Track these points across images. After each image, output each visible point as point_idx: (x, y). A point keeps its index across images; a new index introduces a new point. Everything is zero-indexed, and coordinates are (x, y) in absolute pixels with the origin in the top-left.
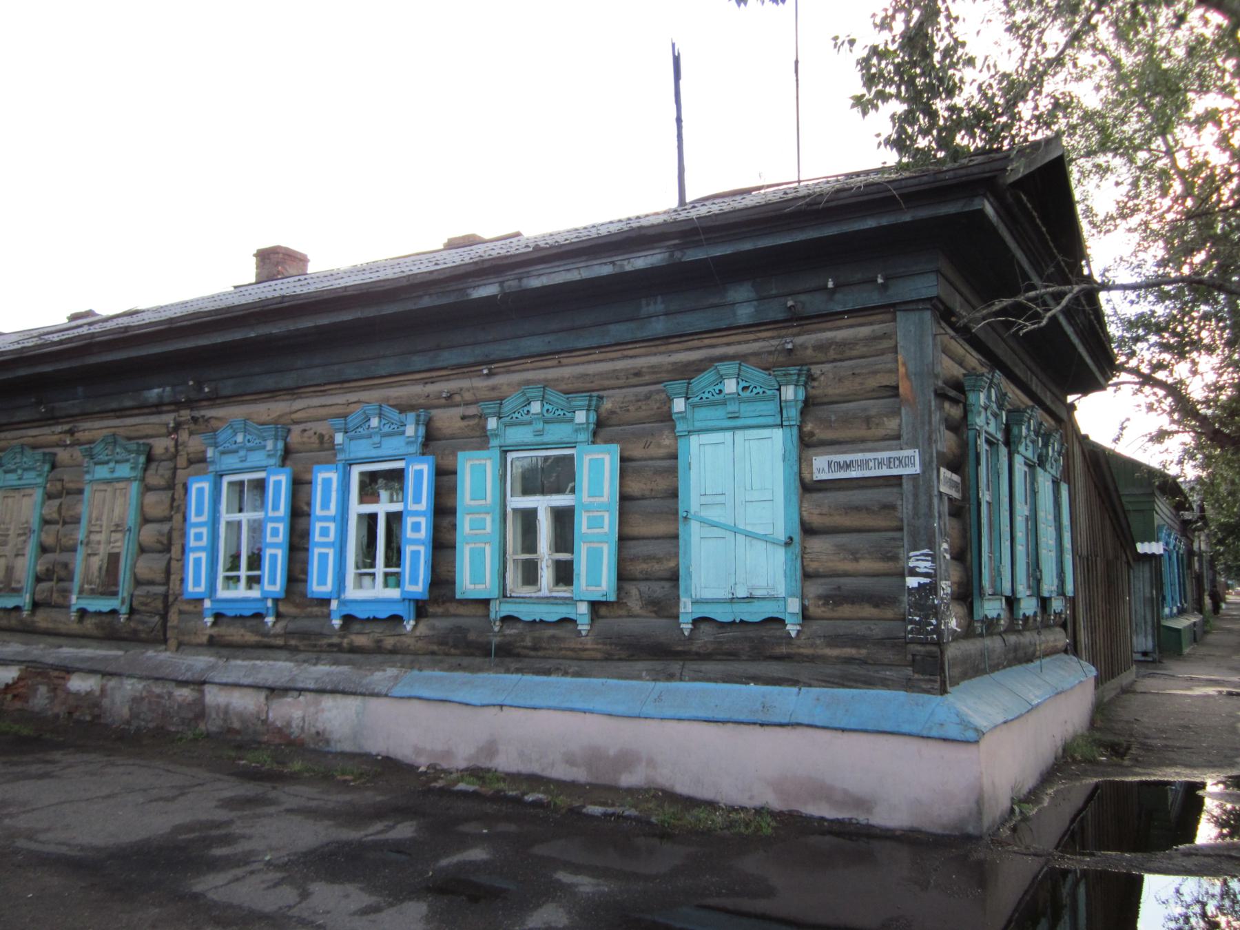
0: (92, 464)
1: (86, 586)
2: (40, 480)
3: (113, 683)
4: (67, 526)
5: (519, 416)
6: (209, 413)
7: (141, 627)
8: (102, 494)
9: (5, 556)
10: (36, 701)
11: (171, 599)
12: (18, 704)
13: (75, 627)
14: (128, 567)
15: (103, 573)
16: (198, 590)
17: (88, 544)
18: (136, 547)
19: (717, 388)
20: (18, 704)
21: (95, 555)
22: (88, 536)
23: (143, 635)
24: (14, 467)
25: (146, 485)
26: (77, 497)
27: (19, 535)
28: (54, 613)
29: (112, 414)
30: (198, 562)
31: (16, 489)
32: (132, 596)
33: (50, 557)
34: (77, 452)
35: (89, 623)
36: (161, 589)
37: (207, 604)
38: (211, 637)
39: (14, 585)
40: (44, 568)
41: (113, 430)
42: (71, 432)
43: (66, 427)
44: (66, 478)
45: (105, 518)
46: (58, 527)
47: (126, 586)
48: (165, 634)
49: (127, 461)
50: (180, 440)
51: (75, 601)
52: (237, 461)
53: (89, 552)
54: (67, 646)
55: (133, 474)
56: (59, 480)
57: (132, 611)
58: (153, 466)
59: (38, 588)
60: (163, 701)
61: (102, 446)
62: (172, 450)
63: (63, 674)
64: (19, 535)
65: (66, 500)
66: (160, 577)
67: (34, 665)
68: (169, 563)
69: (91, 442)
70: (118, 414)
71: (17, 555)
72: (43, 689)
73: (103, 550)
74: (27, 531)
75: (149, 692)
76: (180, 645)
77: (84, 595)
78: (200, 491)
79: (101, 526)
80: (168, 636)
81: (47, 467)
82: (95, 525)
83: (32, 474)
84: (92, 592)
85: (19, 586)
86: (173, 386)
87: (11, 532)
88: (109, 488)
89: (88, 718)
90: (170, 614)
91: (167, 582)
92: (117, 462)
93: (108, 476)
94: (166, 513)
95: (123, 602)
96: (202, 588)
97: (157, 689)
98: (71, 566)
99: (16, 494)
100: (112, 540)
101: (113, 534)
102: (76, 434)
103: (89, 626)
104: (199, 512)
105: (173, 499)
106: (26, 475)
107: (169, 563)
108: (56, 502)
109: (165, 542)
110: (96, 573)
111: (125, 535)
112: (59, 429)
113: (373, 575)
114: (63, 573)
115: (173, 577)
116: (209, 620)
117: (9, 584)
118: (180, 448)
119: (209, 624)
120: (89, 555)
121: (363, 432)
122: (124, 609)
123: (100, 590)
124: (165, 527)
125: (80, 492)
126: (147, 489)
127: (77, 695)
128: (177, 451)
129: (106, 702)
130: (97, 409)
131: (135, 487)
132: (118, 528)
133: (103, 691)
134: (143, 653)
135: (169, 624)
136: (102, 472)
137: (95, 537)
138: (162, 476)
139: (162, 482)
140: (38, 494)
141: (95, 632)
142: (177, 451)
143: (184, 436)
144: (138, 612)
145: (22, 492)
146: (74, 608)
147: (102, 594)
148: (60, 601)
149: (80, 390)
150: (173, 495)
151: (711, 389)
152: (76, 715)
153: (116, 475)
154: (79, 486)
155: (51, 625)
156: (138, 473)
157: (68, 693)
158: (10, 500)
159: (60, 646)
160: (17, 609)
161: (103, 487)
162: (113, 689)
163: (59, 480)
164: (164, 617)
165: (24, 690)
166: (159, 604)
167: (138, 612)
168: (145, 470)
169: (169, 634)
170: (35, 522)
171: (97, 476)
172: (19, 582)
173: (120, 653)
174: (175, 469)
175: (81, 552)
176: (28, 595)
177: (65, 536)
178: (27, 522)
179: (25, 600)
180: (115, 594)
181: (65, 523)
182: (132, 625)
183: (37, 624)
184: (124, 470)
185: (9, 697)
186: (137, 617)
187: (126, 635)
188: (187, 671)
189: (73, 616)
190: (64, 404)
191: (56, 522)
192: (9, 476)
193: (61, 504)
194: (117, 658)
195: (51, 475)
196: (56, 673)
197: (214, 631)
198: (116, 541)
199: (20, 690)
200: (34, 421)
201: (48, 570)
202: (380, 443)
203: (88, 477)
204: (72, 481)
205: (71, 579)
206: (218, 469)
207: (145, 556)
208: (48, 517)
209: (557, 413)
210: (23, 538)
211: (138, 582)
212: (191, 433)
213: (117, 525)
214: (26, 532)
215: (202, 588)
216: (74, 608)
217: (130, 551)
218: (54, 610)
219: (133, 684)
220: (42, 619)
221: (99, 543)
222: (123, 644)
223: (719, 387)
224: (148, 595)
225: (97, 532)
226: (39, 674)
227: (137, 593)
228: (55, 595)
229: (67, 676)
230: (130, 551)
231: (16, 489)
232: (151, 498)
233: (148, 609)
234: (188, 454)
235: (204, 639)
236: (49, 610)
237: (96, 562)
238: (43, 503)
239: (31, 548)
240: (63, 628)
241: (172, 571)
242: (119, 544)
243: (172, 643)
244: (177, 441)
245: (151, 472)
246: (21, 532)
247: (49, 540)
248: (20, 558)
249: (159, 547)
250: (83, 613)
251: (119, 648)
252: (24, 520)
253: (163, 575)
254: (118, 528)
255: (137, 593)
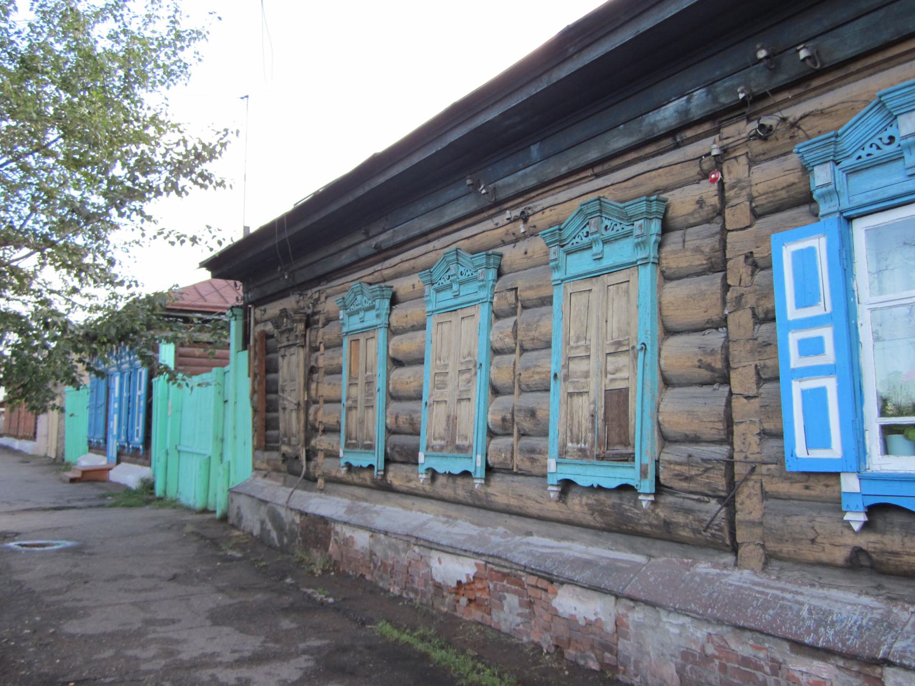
0: (562, 255)
1: (569, 445)
2: (483, 294)
3: (638, 615)
4: (525, 354)
5: (873, 150)
6: (794, 112)
7: (680, 519)
8: (584, 297)
9: (446, 402)
10: (502, 615)
11: (740, 470)
12: (477, 615)
13: (553, 508)
14: (648, 411)
15: (599, 423)
16: (819, 454)
17: (566, 377)
18: (657, 378)
19: (885, 136)
20: (477, 615)
21: (580, 394)
22: (566, 366)
23: (685, 533)
24: (448, 282)
25: (662, 272)
26: (544, 309)
27: (461, 372)
28: (519, 484)
29: (589, 173)
30: (814, 400)
31: (452, 310)
32: (657, 462)
33: (504, 401)
34: (537, 245)
35: (577, 505)
36: (721, 451)
37: (850, 484)
38: (858, 551)
39: (458, 442)
40: (499, 418)
41: (454, 247)
42: (524, 218)
43: (517, 213)
44: (520, 284)
45: (592, 333)
46: (513, 357)
47: (647, 444)
48: (733, 534)
49: (627, 235)
50: (727, 180)
51: (555, 470)
52: (900, 178)
53: (571, 390)
54: (540, 534)
55: (641, 254)
56: (512, 289)
57: (660, 488)
58: (675, 237)
59: (491, 447)
60: (759, 674)
61: (578, 221)
62: (715, 200)
63: (543, 584)
64: (461, 372)
65: (523, 317)
66: (715, 428)
67: (497, 561)
68: (729, 404)
69: (428, 267)
70: (597, 170)
71: (460, 400)
72: (512, 600)
73: (596, 387)
74: (471, 366)
75: (723, 648)
76: (770, 557)
77: (568, 459)
78: (805, 259)
79: (587, 348)
80: (739, 540)
81: (492, 274)
82: (577, 347)
83: (473, 287)
84: (583, 453)
85: (466, 443)
86: (709, 85)
87: (449, 370)
88: (596, 286)
89: (594, 665)
90: (738, 500)
91: (728, 439)
92: (605, 242)
93: (594, 266)
94: (714, 314)
95: (644, 474)
96: (835, 451)
97: (743, 647)
98: (540, 414)
99: (453, 317)
100: (609, 368)
101: (609, 358)
102: (531, 219)
103: (577, 508)
104: (806, 297)
105: (726, 287)
106: (464, 290)
107: (729, 404)
108: (510, 321)
109: (719, 365)
110: (586, 424)
111: (636, 357)
112: (502, 219)
113: (883, 413)
114: (527, 425)
115: (737, 429)
116: (857, 519)
117: (453, 440)
118: (729, 194)
119: (856, 527)
120: (571, 395)
121: (445, 283)
122: (647, 486)
123: (596, 451)
124: (715, 339)
125: (547, 301)
126: (667, 277)
127: (571, 621)
128: (723, 200)
129: (625, 646)
130: (564, 170)
131: (646, 276)
132: (618, 348)
133: (618, 623)
134: (688, 567)
135: (739, 516)
136: (581, 263)
137: (577, 367)
138: (698, 250)
139: (699, 261)
140: (483, 313)
141: (588, 519)
142: (723, 200)
143: (736, 170)
144: (671, 491)
145: (461, 314)
146: (552, 480)
147: (600, 458)
148: (526, 466)
149: (535, 151)
150: (725, 278)
151: (876, 141)
152: (570, 653)
153: (605, 263)
154: (544, 293)
155: (514, 502)
156: (650, 251)
157: (555, 614)
158: (445, 327)
159: (529, 534)
160: (466, 474)
161: (585, 286)
162: (639, 625)
163: (512, 289)
164: (729, 502)
165: (485, 596)
166: (720, 483)
167: (671, 491)
168: (660, 245)
169: (741, 535)
170: (481, 355)
171: (572, 271)
172: (466, 438)
173: (640, 559)
174: (724, 231)
175: (558, 389)
176: (479, 457)
177: (527, 369)
178: (469, 354)
179: (476, 464)
180: (628, 458)
181: (523, 350)
182: (662, 513)
183: (493, 498)
184: (622, 252)
185: (463, 601)
186: (669, 499)
187: (647, 529)
188: (820, 623)
189: (553, 492)
190: (509, 179)
191: (513, 351)
192: (442, 296)
193: (515, 323)
194: (635, 568)
195: (497, 285)
196: (532, 580)
197: (867, 541)
198: (617, 370)
199: (478, 595)
200: (482, 211)
201: (504, 420)
202: (602, 251)
203: (556, 276)
204: (531, 288)
205: (545, 434)
206: (845, 205)
207: (671, 392)
208: (497, 345)
209: (616, 229)
210: (467, 376)
211: (665, 439)
212: (753, 162)
213: (619, 343)
214: (469, 368)
215: (835, 451)
216: (552, 480)
217: (648, 383)
218: (516, 478)
219: (683, 626)
220: (397, 476)
221: (586, 375)
222: (638, 541)
223: (891, 131)
224: (690, 461)
225: (581, 358)
226: (505, 576)
227: (664, 457)
228: (518, 458)
229: (550, 588)
230: (648, 383)
231: (452, 310)
232: (675, 291)
233: (692, 486)
234: (751, 199)
235: (840, 555)
236: (509, 478)
237: (583, 406)
238: (490, 325)
239: (478, 390)
240: (533, 507)
241: (736, 417)
242: (624, 374)
243: (751, 552)
244: (721, 183)
245: (667, 249)
246: (463, 368)
247: (503, 378)
248: (463, 403)
249: (705, 374)
250: (567, 485)
251: (635, 551)
252: (466, 352)
253: (720, 426)
254: (618, 348)
255: (664, 457)
